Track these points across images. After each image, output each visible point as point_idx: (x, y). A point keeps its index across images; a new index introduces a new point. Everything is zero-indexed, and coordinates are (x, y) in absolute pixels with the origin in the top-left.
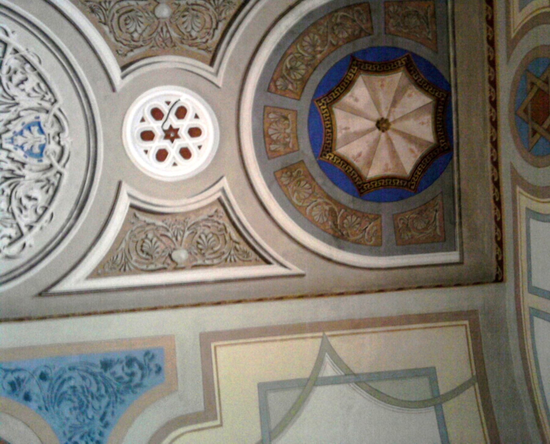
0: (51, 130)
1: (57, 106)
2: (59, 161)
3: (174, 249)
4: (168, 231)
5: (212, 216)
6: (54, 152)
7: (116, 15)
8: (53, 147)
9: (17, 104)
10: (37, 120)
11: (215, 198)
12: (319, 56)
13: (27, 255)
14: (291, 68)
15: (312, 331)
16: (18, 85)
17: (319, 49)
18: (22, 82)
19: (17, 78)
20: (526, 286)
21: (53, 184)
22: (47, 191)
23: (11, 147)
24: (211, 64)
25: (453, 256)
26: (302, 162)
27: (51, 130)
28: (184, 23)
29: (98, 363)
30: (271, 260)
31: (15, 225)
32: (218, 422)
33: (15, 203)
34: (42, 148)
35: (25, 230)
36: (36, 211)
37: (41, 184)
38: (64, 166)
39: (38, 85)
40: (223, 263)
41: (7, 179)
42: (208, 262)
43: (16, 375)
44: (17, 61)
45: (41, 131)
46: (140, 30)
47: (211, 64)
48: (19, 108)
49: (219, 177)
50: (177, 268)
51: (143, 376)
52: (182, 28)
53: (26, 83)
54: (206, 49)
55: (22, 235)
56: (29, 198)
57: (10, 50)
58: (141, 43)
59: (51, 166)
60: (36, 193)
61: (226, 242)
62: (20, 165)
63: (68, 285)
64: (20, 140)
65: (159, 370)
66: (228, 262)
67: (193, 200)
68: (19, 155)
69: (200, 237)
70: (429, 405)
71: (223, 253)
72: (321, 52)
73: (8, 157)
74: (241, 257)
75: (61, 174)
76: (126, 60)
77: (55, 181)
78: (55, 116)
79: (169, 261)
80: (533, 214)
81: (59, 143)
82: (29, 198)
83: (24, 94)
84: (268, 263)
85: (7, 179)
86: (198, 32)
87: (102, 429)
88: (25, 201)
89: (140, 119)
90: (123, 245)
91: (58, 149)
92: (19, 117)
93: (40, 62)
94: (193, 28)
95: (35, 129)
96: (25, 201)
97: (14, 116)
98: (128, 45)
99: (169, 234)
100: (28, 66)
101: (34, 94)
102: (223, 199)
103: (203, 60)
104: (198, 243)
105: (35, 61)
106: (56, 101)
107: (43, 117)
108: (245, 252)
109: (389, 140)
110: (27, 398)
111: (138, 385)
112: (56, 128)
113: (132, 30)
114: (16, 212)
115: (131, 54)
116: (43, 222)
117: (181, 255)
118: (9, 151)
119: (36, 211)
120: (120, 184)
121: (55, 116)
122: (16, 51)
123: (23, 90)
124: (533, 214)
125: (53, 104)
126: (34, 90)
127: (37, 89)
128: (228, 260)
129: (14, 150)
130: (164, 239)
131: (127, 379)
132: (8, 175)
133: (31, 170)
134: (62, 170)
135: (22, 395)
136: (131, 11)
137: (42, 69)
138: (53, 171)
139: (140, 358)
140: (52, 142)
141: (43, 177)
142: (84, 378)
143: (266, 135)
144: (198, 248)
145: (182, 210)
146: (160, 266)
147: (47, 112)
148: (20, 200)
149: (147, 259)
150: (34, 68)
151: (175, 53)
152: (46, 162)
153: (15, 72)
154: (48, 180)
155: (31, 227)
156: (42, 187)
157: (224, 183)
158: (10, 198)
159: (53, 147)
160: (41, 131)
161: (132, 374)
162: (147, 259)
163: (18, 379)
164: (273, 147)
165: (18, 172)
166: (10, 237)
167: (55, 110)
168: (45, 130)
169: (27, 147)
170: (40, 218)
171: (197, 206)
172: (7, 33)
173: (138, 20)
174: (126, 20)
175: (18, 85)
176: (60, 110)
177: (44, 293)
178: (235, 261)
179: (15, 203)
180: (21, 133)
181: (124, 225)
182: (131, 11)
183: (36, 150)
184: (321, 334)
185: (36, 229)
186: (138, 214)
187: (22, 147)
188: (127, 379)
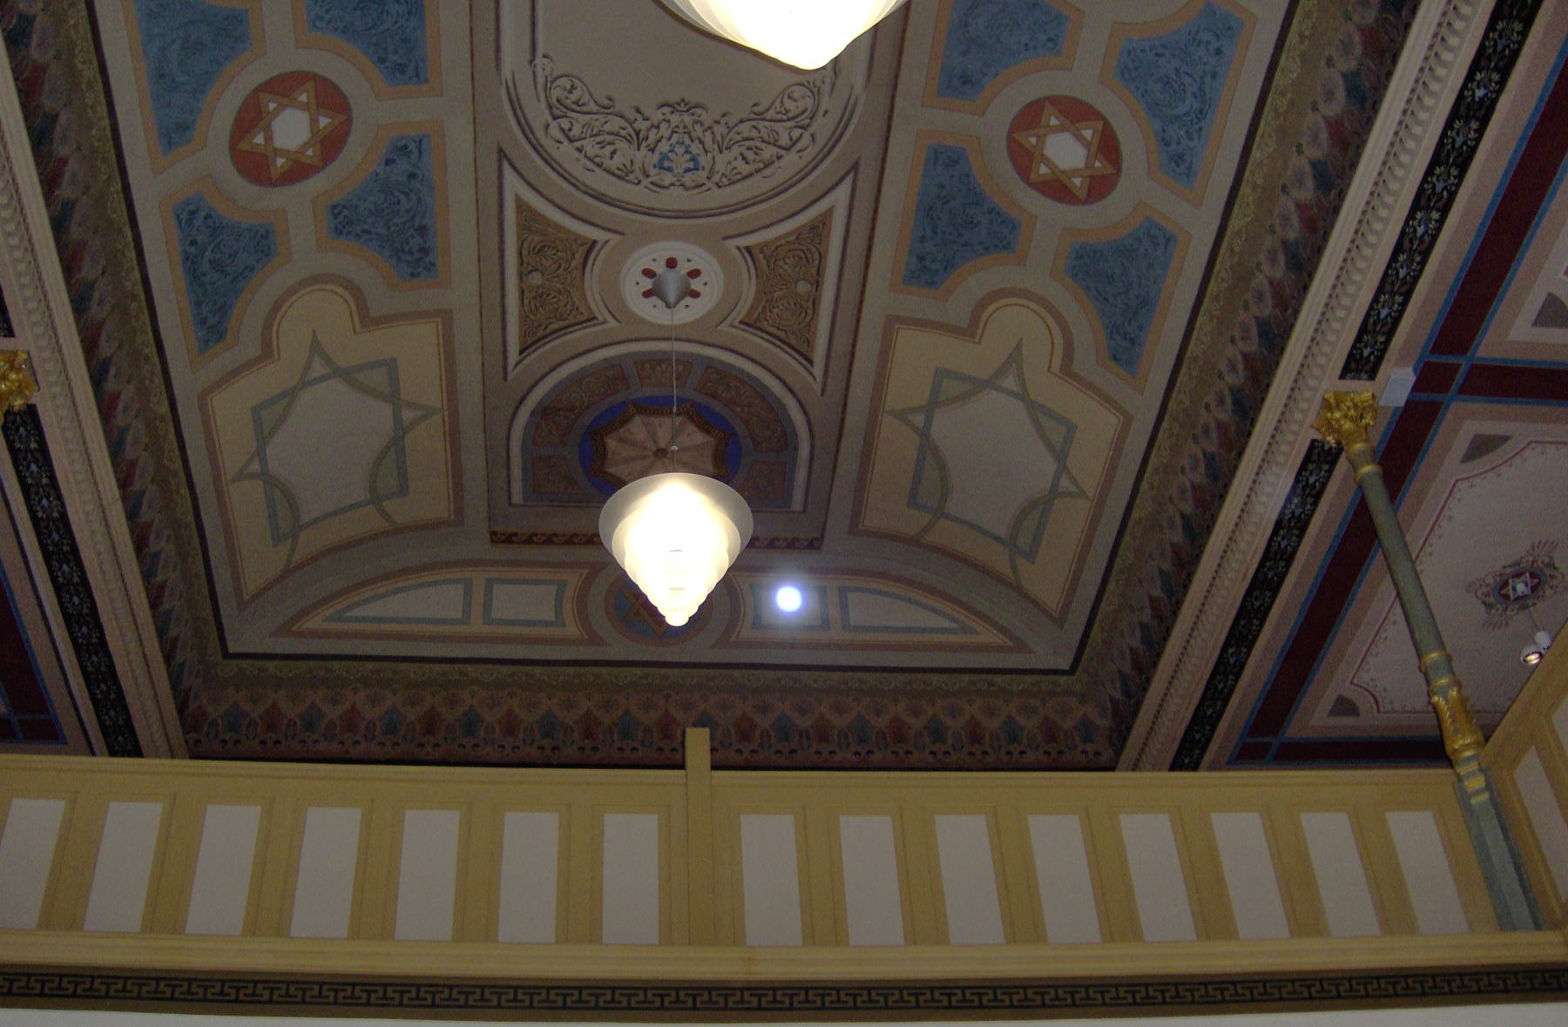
1: (714, 187)
2: (652, 183)
3: (543, 275)
4: (565, 270)
5: (577, 309)
6: (662, 180)
8: (668, 179)
9: (721, 152)
11: (597, 315)
12: (738, 409)
13: (547, 143)
14: (729, 387)
15: (449, 401)
16: (741, 154)
17: (746, 409)
18: (744, 158)
19: (750, 155)
20: (496, 575)
21: (627, 175)
22: (618, 169)
25: (517, 498)
26: (629, 388)
28: (789, 303)
29: (424, 222)
31: (583, 136)
32: (358, 329)
33: (610, 138)
34: (669, 170)
35: (578, 144)
36: (596, 156)
37: (628, 165)
38: (646, 187)
41: (638, 134)
42: (526, 301)
43: (416, 152)
44: (769, 156)
45: (688, 170)
46: (786, 267)
47: (741, 322)
48: (716, 152)
49: (620, 230)
50: (521, 276)
51: (407, 262)
52: (784, 302)
53: (744, 162)
54: (758, 319)
55: (571, 141)
56: (614, 153)
57: (782, 152)
58: (772, 266)
59: (648, 176)
60: (618, 159)
61: (547, 318)
62: (652, 146)
63: (509, 176)
64: (680, 150)
65: (413, 275)
66: (524, 318)
67: (597, 297)
68: (664, 147)
69: (555, 297)
71: (535, 315)
72: (743, 411)
73: (662, 137)
76: (756, 252)
77: (631, 177)
78: (703, 185)
79: (530, 268)
80: (562, 586)
81: (672, 185)
82: (614, 153)
83: (732, 159)
84: (521, 352)
85: (638, 134)
87: (354, 233)
88: (609, 149)
90: (552, 230)
91: (666, 183)
92: (706, 151)
93: (764, 177)
95: (691, 165)
96: (609, 149)
97: (707, 146)
98: (771, 256)
99: (560, 271)
100: (761, 165)
101: (730, 167)
103: (749, 314)
104: (548, 295)
105: (767, 172)
106: (719, 187)
107: (704, 174)
108: (534, 334)
109: (645, 457)
110: (388, 162)
111: (399, 259)
112: (688, 183)
113: (787, 261)
114: (598, 139)
115: (761, 256)
116: (584, 161)
117: (536, 279)
118: (669, 139)
119: (596, 156)
120: (622, 234)
121: (703, 185)
122: (779, 157)
123: (736, 159)
124: (562, 586)
125: (717, 184)
130: (555, 266)
131: (407, 248)
132: (642, 135)
133: (645, 156)
135: (391, 157)
136: (808, 261)
137: (758, 177)
138: (641, 178)
139: (427, 259)
140: (674, 179)
141: (636, 167)
142: (408, 211)
143: (660, 362)
144: (543, 294)
145: (587, 285)
146: (525, 260)
147: (708, 178)
148: (613, 144)
149: (534, 249)
150: (758, 171)
151: (757, 292)
152: (652, 172)
153: (756, 154)
154: (632, 172)
155: (580, 150)
156: (625, 165)
157: (612, 323)
158: (617, 135)
160: (688, 170)
161: (410, 252)
162: (534, 249)
163: (411, 152)
164: (647, 366)
165: (644, 144)
166: (570, 130)
167: (709, 185)
168: (689, 174)
173: (795, 267)
175: (741, 154)
177: (502, 154)
180: (687, 152)
181: (574, 234)
182: (808, 261)
183: (666, 164)
184: (446, 408)
185: (577, 154)
186: (585, 248)
187: (672, 151)
188: (407, 248)
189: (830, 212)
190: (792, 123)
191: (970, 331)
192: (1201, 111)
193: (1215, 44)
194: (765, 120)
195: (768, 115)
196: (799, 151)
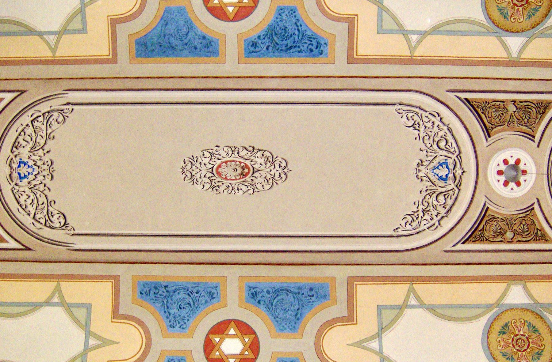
0: (15, 175)
1: (11, 187)
2: (12, 159)
7: (532, 233)
8: (15, 166)
9: (30, 188)
10: (21, 180)
13: (30, 113)
23: (34, 167)
24: (488, 208)
27: (15, 175)
30: (465, 101)
31: (35, 127)
33: (34, 139)
34: (19, 166)
39: (19, 197)
40: (490, 102)
45: (19, 174)
50: (514, 102)
55: (32, 121)
57: (32, 215)
64: (30, 170)
70: (139, 10)
74: (480, 104)
75: (12, 152)
77: (14, 149)
78: (13, 182)
84: (466, 99)
86: (493, 224)
89: (526, 181)
92: (29, 183)
94: (496, 226)
95: (22, 175)
102: (487, 137)
103: (492, 211)
114: (33, 134)
117: (512, 108)
121: (13, 182)
122: (29, 215)
126: (22, 195)
127: (20, 195)
128: (485, 103)
129: (33, 165)
134: (11, 154)
152: (18, 159)
155: (27, 125)
159: (15, 166)
160: (19, 174)
165: (32, 154)
167: (13, 184)
168: (17, 175)
169: (26, 166)
170: (23, 130)
171: (503, 133)
172: (33, 223)
174: (528, 230)
176: (10, 184)
178: (483, 102)
179: (34, 139)
180: (29, 173)
183: (22, 165)
187: (29, 166)
189: (7, 242)
190: (47, 218)
191: (116, 314)
192: (184, 289)
193: (313, 48)
194: (48, 206)
195: (50, 208)
196: (33, 223)
